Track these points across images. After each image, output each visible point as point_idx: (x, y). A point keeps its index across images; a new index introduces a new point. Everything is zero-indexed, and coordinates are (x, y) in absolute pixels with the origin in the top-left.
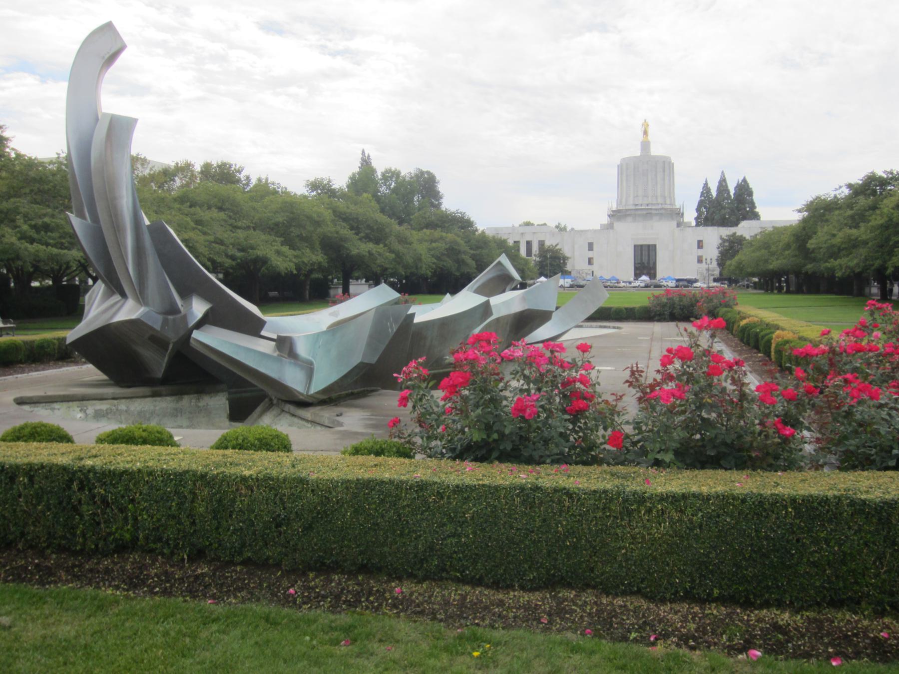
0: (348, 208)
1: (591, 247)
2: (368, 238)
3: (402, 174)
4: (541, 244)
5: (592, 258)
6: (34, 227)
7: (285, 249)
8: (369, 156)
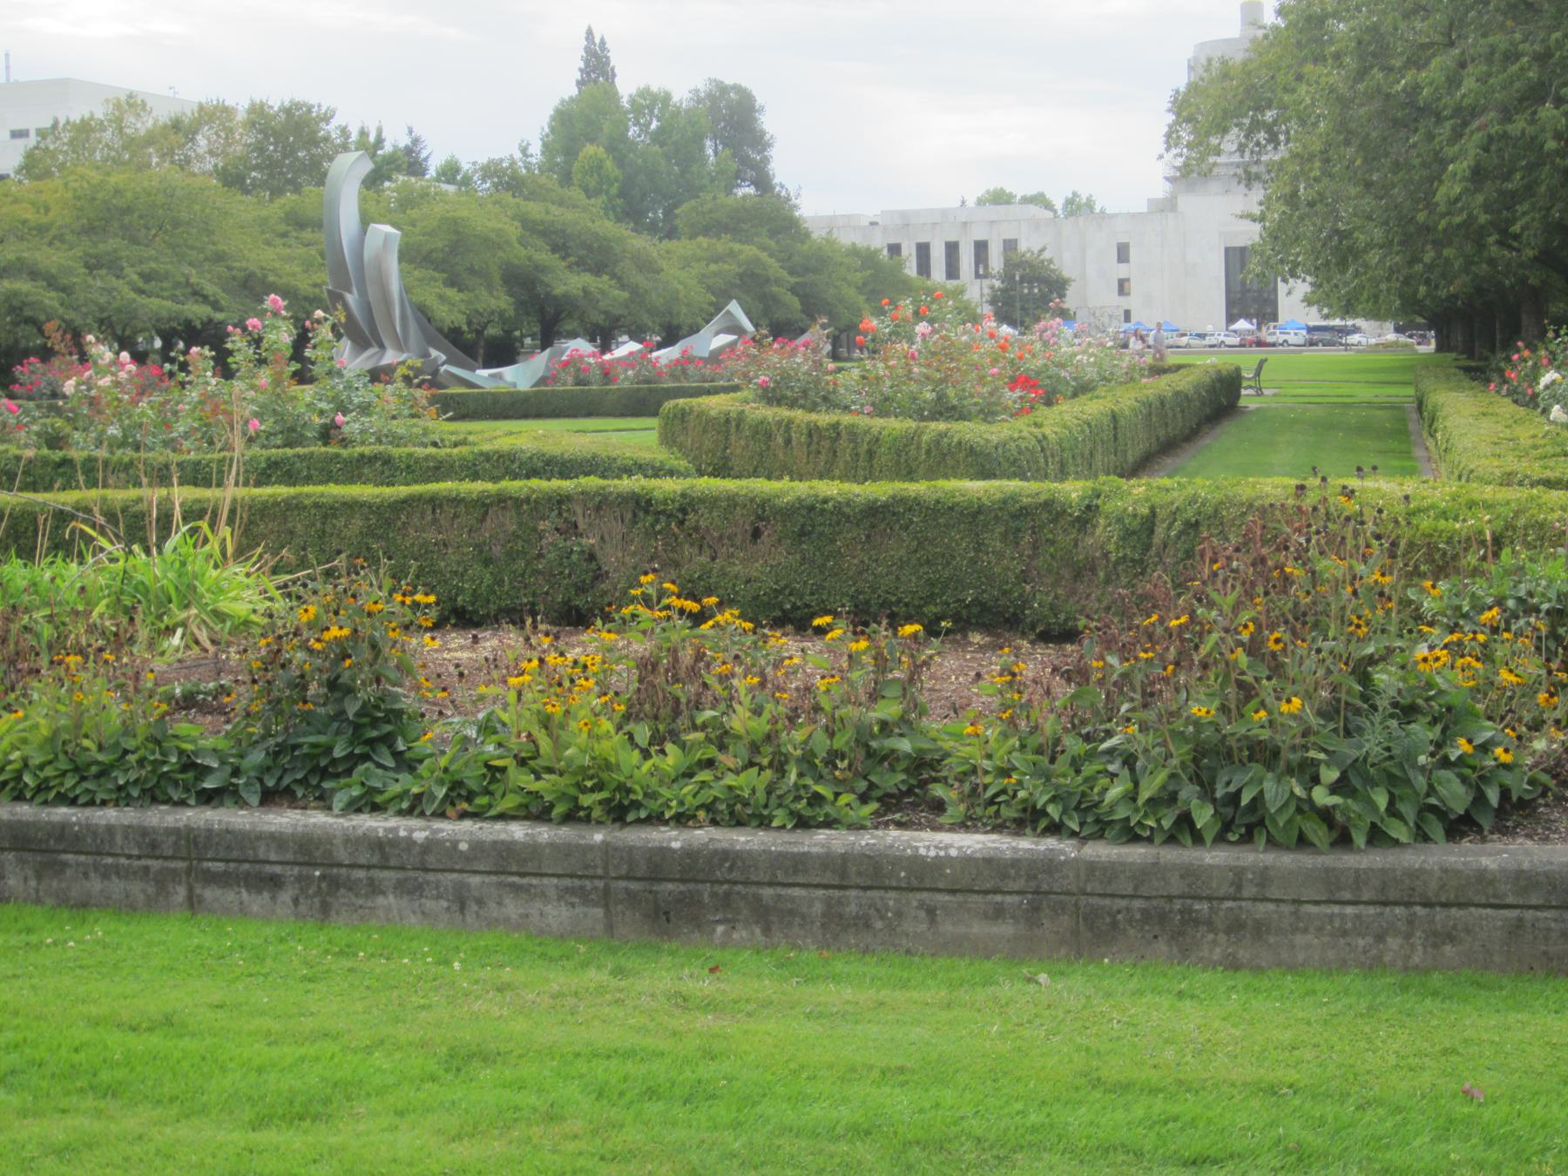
0: (548, 212)
1: (1123, 254)
2: (581, 265)
3: (676, 98)
4: (1010, 245)
5: (1128, 280)
6: (141, 275)
7: (451, 293)
8: (603, 42)
